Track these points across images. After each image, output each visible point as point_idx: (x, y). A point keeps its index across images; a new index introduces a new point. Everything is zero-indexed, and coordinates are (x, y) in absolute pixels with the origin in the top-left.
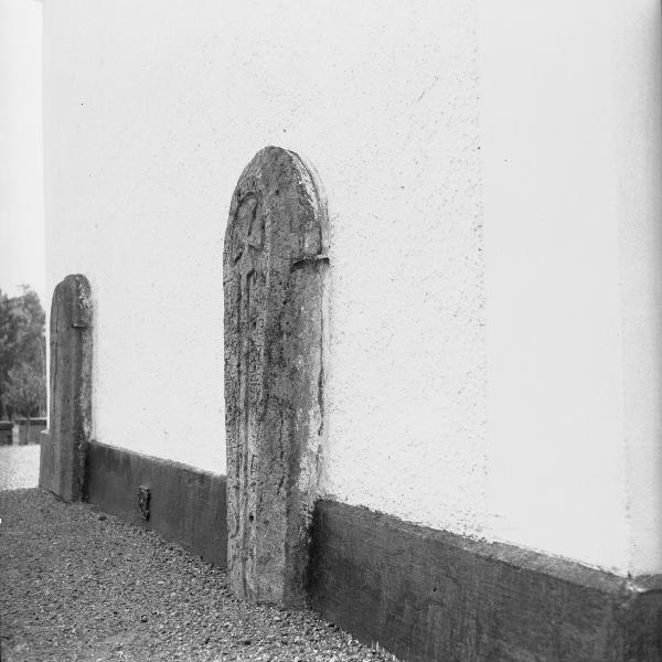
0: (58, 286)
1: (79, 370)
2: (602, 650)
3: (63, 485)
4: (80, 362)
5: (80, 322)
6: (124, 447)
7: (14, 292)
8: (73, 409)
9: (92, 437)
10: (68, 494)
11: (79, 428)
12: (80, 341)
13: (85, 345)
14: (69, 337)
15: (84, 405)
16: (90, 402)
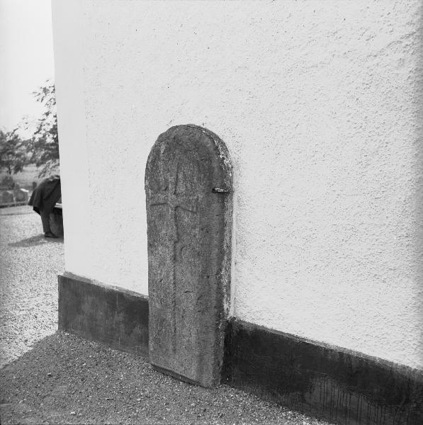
0: (161, 136)
1: (222, 241)
2: (124, 331)
3: (200, 371)
4: (222, 231)
5: (223, 186)
6: (341, 345)
7: (7, 129)
8: (215, 286)
9: (231, 314)
10: (208, 378)
11: (220, 307)
12: (223, 208)
13: (227, 212)
14: (209, 205)
15: (225, 281)
16: (229, 276)
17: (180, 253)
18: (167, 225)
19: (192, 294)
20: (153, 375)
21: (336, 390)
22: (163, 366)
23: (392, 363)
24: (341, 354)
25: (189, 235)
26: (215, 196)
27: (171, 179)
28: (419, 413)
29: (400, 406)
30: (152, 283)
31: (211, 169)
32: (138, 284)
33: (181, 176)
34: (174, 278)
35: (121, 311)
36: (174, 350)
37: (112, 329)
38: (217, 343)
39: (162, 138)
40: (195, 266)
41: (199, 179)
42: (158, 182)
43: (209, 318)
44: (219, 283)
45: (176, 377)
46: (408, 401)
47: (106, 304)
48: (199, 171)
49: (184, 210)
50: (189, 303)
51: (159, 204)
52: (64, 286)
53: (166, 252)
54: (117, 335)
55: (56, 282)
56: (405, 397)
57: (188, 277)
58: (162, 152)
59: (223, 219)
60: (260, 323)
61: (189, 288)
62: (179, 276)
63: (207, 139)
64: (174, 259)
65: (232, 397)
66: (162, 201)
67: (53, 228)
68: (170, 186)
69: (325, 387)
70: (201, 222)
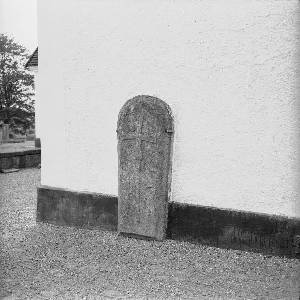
3: (157, 232)
5: (171, 129)
10: (161, 235)
11: (167, 196)
12: (171, 141)
15: (169, 181)
17: (145, 166)
18: (135, 151)
19: (152, 189)
20: (122, 238)
21: (237, 232)
22: (130, 232)
23: (268, 214)
24: (240, 213)
25: (150, 156)
26: (167, 135)
27: (138, 125)
28: (282, 237)
29: (272, 235)
30: (123, 186)
31: (165, 119)
32: (109, 186)
33: (145, 124)
34: (140, 181)
35: (90, 206)
36: (139, 222)
37: (83, 217)
38: (165, 216)
39: (130, 102)
40: (154, 173)
41: (158, 125)
42: (128, 127)
43: (162, 202)
44: (167, 182)
45: (139, 237)
46: (277, 232)
47: (78, 203)
48: (158, 121)
49: (147, 142)
50: (150, 194)
51: (130, 139)
52: (42, 195)
53: (134, 166)
54: (87, 221)
55: (35, 195)
56: (275, 230)
57: (150, 179)
58: (132, 110)
59: (170, 147)
60: (190, 203)
61: (149, 185)
62: (143, 179)
63: (161, 104)
64: (140, 170)
65: (174, 244)
66: (131, 138)
67: (143, 128)
68: (138, 129)
69: (231, 232)
70: (159, 149)
